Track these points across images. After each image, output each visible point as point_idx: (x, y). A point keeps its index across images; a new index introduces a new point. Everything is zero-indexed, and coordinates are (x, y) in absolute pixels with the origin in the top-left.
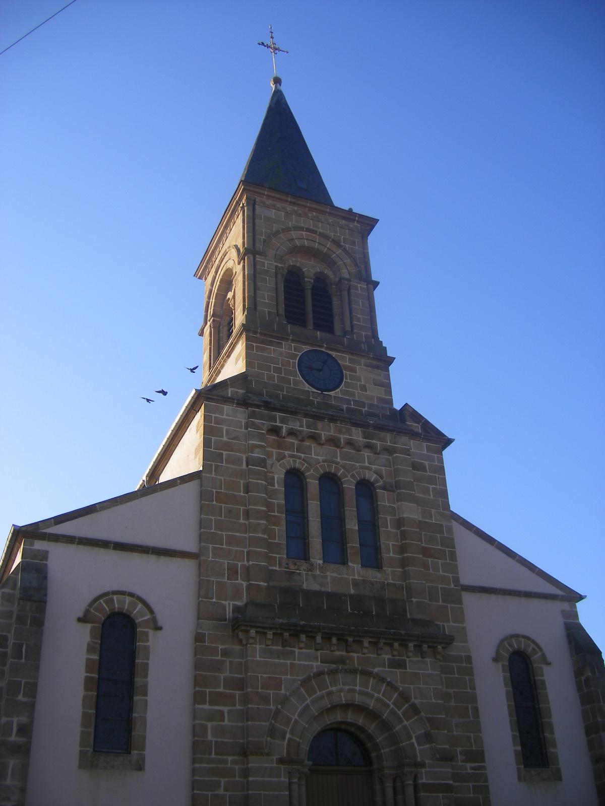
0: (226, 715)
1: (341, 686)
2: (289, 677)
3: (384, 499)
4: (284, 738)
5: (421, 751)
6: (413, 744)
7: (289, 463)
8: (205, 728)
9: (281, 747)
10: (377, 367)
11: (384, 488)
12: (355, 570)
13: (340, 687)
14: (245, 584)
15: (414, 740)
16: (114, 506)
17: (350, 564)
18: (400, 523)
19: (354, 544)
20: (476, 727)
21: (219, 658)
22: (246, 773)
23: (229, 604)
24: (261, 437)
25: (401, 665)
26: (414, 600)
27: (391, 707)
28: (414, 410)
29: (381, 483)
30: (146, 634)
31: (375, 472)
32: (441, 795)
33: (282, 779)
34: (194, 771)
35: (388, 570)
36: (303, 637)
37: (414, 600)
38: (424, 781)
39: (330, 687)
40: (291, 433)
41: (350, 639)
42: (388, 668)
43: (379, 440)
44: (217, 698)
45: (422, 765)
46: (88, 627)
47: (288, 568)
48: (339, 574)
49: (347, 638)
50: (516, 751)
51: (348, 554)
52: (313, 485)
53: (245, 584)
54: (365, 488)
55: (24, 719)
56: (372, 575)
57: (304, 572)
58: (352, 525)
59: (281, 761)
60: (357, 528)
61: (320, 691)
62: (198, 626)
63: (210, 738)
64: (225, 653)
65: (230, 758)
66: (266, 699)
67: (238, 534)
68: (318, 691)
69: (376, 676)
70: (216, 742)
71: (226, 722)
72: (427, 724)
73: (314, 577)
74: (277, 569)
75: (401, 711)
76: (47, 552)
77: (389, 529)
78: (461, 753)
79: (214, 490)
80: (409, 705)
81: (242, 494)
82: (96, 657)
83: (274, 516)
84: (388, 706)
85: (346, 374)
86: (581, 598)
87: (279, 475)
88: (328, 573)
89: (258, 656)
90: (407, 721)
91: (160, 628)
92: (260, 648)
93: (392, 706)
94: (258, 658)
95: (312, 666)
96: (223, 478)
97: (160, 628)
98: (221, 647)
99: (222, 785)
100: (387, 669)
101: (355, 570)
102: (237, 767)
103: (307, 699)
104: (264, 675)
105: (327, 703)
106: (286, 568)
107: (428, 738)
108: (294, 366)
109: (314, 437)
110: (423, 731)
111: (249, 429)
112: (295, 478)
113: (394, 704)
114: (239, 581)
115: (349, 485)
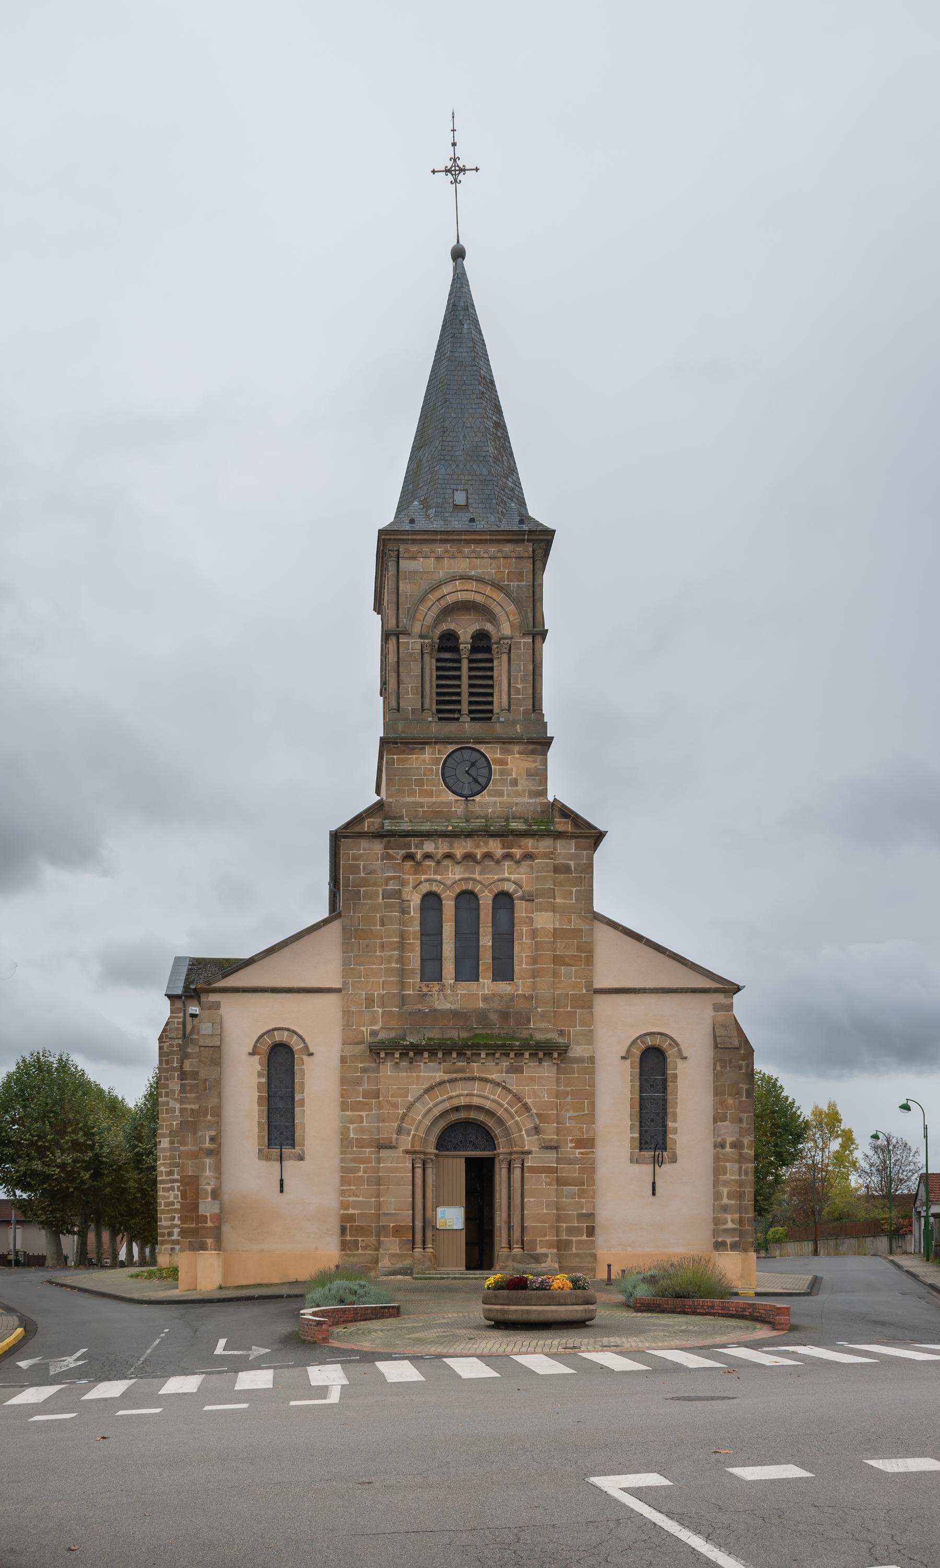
0: (364, 1118)
1: (461, 1091)
2: (415, 1086)
3: (521, 909)
4: (409, 1134)
5: (530, 1143)
6: (522, 1136)
7: (425, 888)
8: (348, 1128)
9: (406, 1142)
10: (533, 752)
11: (522, 898)
12: (487, 985)
14: (380, 1010)
15: (524, 1132)
16: (270, 954)
17: (481, 980)
18: (534, 933)
19: (486, 958)
20: (591, 1118)
21: (359, 1074)
22: (379, 1160)
23: (367, 1029)
24: (395, 867)
25: (519, 1070)
26: (539, 1010)
28: (563, 805)
29: (520, 894)
30: (302, 1060)
31: (514, 883)
32: (544, 1175)
33: (407, 1164)
34: (342, 1160)
35: (518, 981)
36: (426, 1055)
37: (539, 1010)
38: (530, 1164)
40: (427, 856)
41: (469, 1053)
43: (520, 847)
44: (357, 1106)
45: (529, 1153)
46: (257, 1058)
47: (421, 991)
48: (469, 991)
50: (675, 1121)
51: (480, 971)
52: (449, 906)
53: (380, 1010)
54: (504, 900)
55: (213, 1133)
56: (503, 987)
57: (436, 993)
58: (486, 940)
59: (407, 1152)
60: (490, 943)
62: (342, 1051)
63: (352, 1136)
64: (364, 1070)
65: (368, 1150)
66: (395, 1106)
67: (374, 966)
69: (492, 1082)
70: (357, 1138)
71: (365, 1124)
72: (537, 1120)
73: (445, 997)
74: (411, 993)
76: (220, 1002)
77: (524, 941)
78: (571, 1141)
79: (353, 928)
81: (378, 928)
82: (264, 1080)
83: (409, 943)
84: (503, 1105)
85: (495, 769)
86: (738, 989)
87: (415, 900)
88: (459, 991)
91: (312, 1054)
93: (506, 1105)
94: (389, 1073)
95: (435, 1077)
96: (360, 915)
97: (312, 1054)
98: (360, 1065)
99: (362, 1169)
101: (487, 985)
102: (373, 1156)
103: (430, 1103)
105: (447, 1105)
106: (419, 991)
107: (537, 1130)
108: (437, 774)
109: (449, 856)
111: (385, 861)
112: (431, 901)
113: (508, 1103)
114: (376, 1009)
115: (486, 900)
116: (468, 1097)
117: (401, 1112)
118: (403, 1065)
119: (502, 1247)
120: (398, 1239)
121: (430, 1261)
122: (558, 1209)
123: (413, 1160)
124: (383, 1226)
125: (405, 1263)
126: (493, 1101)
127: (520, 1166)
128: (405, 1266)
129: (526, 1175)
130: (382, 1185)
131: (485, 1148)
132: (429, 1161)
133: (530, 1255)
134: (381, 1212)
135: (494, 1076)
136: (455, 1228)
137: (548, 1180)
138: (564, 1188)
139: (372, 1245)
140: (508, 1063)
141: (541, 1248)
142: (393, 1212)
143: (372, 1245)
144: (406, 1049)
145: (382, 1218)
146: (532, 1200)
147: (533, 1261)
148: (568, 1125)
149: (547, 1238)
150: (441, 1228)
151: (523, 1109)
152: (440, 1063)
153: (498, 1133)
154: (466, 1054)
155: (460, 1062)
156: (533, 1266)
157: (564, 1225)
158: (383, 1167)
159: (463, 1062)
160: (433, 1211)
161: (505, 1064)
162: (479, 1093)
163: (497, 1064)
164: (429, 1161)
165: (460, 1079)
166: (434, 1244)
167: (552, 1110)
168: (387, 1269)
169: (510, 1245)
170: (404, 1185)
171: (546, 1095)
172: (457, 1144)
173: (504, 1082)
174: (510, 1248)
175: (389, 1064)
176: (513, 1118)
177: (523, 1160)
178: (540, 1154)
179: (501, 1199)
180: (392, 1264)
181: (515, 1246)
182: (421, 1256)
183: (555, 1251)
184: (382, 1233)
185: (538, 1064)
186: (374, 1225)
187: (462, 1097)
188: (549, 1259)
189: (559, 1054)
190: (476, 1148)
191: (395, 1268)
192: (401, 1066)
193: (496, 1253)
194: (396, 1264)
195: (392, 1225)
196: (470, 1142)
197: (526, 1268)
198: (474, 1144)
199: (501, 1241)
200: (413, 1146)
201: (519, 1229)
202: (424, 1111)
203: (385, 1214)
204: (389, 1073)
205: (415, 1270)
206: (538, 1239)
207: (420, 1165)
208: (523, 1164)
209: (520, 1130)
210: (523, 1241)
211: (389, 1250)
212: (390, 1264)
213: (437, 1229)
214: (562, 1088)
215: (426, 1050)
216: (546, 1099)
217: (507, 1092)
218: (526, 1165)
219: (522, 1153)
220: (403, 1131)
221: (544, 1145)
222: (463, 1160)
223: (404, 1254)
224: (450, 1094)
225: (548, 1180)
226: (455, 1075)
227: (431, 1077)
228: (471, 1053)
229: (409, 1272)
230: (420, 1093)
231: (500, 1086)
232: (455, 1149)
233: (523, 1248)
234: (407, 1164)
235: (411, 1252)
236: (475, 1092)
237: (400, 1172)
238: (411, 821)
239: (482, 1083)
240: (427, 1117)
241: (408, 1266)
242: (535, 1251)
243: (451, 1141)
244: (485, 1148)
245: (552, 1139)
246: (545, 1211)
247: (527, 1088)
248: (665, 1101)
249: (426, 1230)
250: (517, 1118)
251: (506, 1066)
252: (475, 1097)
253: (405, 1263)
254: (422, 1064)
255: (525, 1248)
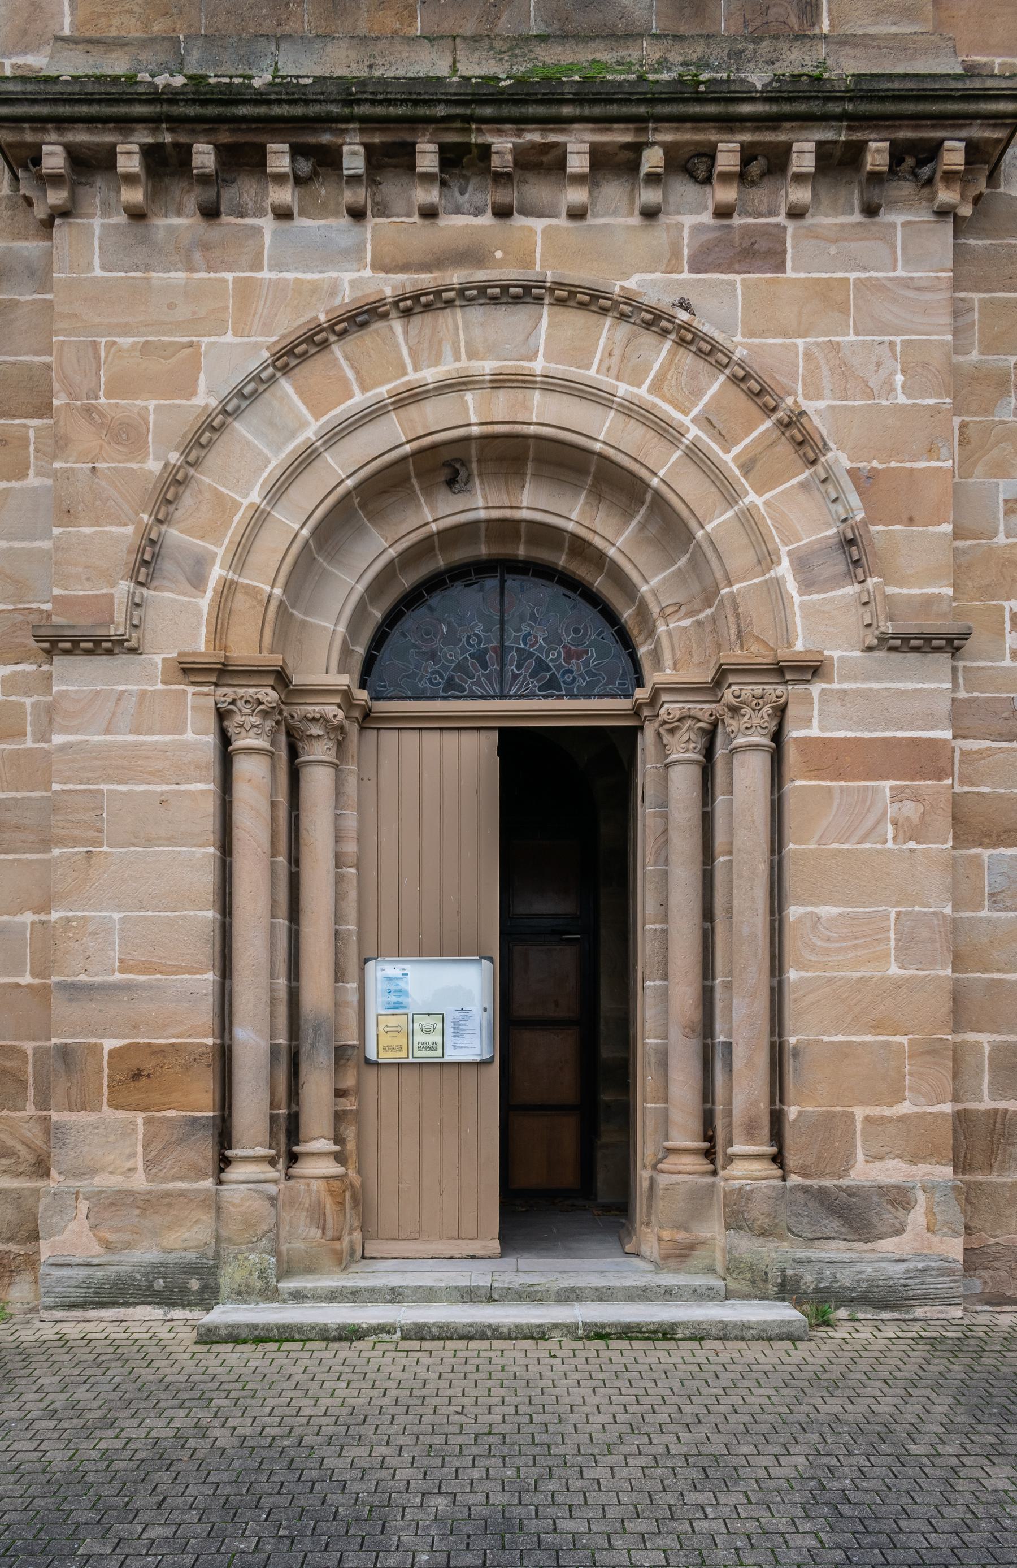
2: (229, 338)
4: (197, 581)
6: (778, 584)
13: (458, 365)
15: (784, 569)
27: (690, 436)
33: (189, 736)
38: (814, 731)
39: (410, 368)
42: (692, 270)
49: (489, 139)
61: (364, 389)
68: (356, 388)
72: (854, 500)
75: (736, 450)
80: (780, 422)
87: (467, 196)
89: (97, 262)
90: (759, 493)
92: (102, 225)
93: (694, 432)
94: (98, 273)
100: (686, 275)
103: (304, 425)
104: (120, 340)
110: (835, 530)
113: (707, 422)
116: (502, 396)
117: (154, 466)
118: (171, 229)
119: (670, 1151)
120: (140, 1117)
121: (320, 1221)
122: (958, 962)
123: (222, 715)
124: (65, 1053)
125: (173, 1239)
126: (631, 410)
127: (766, 741)
128: (171, 1258)
129: (796, 784)
130: (60, 842)
131: (591, 685)
132: (315, 730)
133: (821, 1195)
134: (55, 979)
135: (632, 283)
136: (452, 1055)
137: (910, 810)
138: (986, 853)
139: (22, 1150)
140: (707, 218)
141: (873, 1158)
142: (117, 977)
143: (22, 1150)
144: (175, 122)
145: (61, 1008)
146: (826, 911)
147: (834, 1224)
148: (1001, 539)
149: (905, 1108)
150: (386, 1056)
151: (784, 449)
152: (357, 214)
153: (654, 593)
154: (486, 150)
155: (458, 211)
156: (835, 1250)
157: (985, 1039)
158: (63, 748)
159: (478, 212)
160: (339, 975)
161: (688, 220)
162: (558, 369)
163: (650, 214)
164: (315, 730)
165: (461, 292)
166: (350, 1132)
167: (931, 452)
168: (82, 1273)
169: (710, 1138)
170: (172, 841)
171: (899, 378)
172: (461, 667)
173: (684, 305)
174: (709, 1154)
175: (97, 223)
176: (730, 495)
177: (781, 711)
178: (867, 678)
179: (665, 919)
180: (109, 1247)
181: (737, 1149)
182: (261, 1206)
183: (947, 1171)
184: (60, 1089)
185: (857, 217)
186: (29, 1047)
187: (469, 396)
188: (917, 1217)
189: (974, 151)
190: (551, 687)
191: (124, 1270)
192: (161, 234)
193: (643, 1175)
194: (128, 1246)
195: (109, 1044)
196: (524, 656)
197: (799, 1262)
198: (542, 666)
199: (665, 1119)
200: (219, 630)
201: (762, 1060)
202: (277, 461)
203: (75, 990)
204: (98, 273)
205: (229, 1278)
206: (860, 1113)
207: (263, 743)
208: (777, 736)
209: (768, 559)
210: (777, 1118)
211: (94, 1171)
212: (97, 1249)
213: (368, 1062)
214: (975, 356)
215: (277, 126)
216: (902, 399)
217: (702, 366)
218: (794, 733)
219: (780, 670)
220: (167, 566)
221: (889, 628)
222: (495, 735)
223: (168, 1194)
224: (413, 377)
225: (910, 810)
226: (426, 279)
227: (315, 288)
228: (518, 152)
229: (194, 1284)
230: (252, 365)
231: (665, 332)
232: (453, 689)
233: (778, 1159)
234: (189, 736)
235: (208, 1183)
236: (538, 366)
237: (155, 776)
238: (753, 1282)
239: (575, 320)
240: (295, 493)
241: (191, 1256)
242: (844, 1173)
243: (433, 656)
244: (591, 685)
245: (930, 600)
246: (894, 970)
247: (800, 342)
248: (628, 1141)
249: (304, 1068)
250: (752, 498)
251: (697, 229)
252: (537, 395)
253: (173, 1239)
254: (267, 224)
255: (792, 1160)
